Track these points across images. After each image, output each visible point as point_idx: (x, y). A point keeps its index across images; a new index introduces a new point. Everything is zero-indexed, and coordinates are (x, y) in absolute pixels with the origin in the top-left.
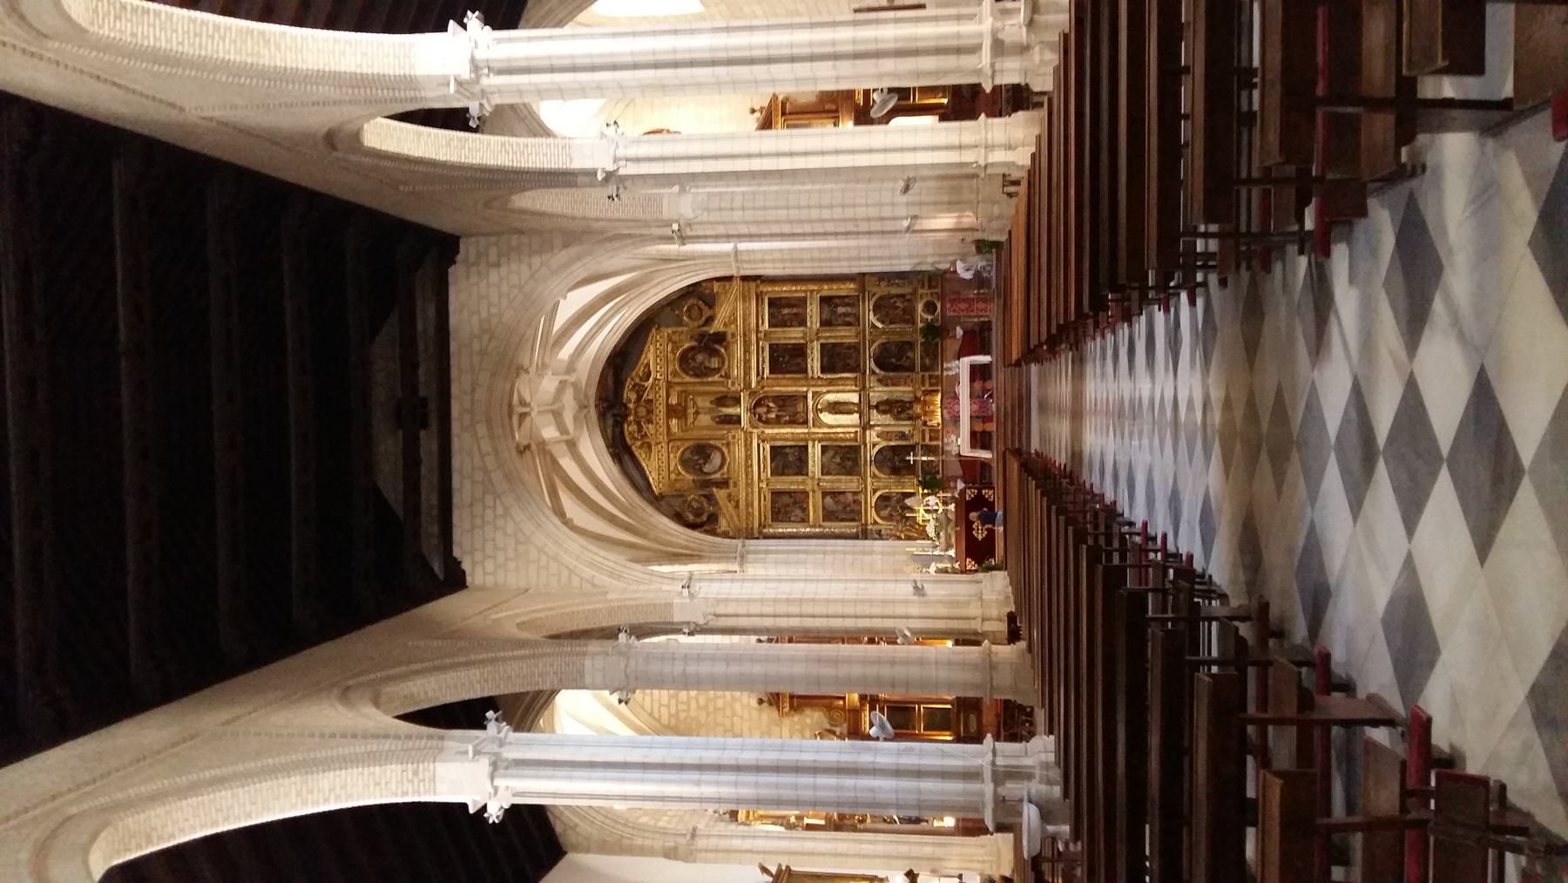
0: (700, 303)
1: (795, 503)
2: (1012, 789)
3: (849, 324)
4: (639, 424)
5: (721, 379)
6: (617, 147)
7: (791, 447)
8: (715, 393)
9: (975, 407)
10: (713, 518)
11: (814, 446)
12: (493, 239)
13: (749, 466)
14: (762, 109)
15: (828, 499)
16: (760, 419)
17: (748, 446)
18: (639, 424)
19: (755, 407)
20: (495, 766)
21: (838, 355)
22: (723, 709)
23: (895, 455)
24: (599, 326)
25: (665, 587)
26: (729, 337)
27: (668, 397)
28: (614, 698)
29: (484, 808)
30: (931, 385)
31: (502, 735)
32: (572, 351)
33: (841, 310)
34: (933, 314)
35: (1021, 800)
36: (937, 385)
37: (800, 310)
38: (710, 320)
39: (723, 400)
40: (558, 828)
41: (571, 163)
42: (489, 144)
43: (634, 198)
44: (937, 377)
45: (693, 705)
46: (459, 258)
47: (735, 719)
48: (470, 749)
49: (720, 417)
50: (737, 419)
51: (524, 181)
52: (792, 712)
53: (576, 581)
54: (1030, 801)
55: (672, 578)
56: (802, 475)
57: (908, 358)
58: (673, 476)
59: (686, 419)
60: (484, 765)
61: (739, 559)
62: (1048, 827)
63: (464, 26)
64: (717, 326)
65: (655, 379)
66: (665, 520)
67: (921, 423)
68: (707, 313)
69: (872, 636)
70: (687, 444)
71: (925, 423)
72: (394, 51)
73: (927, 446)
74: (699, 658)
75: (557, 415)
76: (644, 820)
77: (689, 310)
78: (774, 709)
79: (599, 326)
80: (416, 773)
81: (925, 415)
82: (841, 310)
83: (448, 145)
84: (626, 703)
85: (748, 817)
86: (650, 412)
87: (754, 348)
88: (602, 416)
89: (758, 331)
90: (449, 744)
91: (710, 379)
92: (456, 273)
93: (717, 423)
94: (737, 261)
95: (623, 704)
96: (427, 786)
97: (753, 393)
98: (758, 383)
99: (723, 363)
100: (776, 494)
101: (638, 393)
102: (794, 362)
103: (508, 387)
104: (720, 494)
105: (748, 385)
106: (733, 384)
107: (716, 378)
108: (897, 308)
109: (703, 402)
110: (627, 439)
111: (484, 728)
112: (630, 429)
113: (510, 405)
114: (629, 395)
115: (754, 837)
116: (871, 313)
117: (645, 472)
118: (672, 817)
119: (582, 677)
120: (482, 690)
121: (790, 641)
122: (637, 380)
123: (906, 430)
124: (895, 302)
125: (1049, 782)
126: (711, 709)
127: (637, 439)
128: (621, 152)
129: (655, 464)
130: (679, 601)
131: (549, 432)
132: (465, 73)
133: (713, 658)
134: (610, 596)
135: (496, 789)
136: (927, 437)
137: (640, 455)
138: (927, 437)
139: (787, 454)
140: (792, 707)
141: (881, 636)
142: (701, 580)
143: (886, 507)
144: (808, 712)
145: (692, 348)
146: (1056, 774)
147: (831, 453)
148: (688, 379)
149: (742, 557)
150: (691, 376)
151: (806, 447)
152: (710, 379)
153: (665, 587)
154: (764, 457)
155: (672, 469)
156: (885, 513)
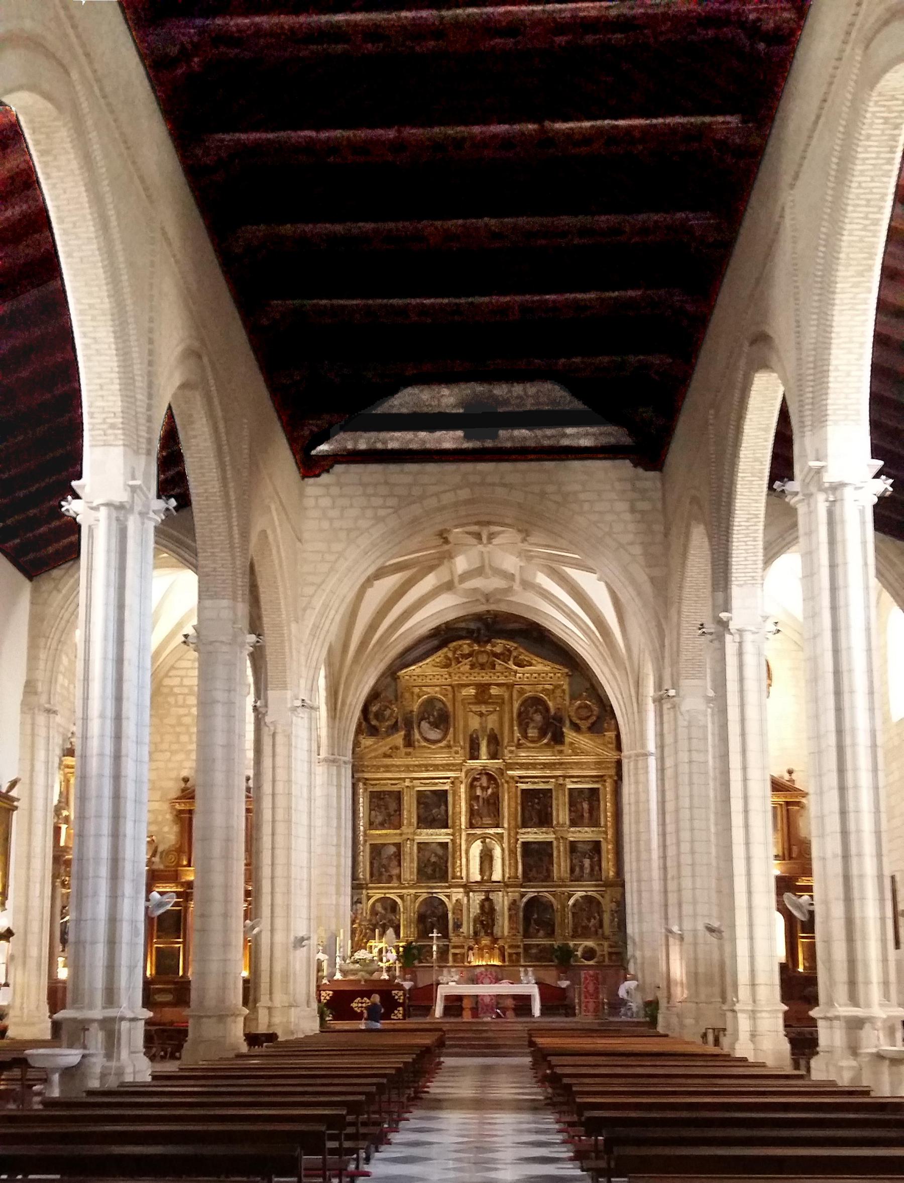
0: (594, 718)
1: (389, 815)
3: (572, 870)
4: (470, 655)
6: (754, 633)
7: (447, 811)
8: (502, 733)
9: (487, 1000)
10: (373, 731)
14: (793, 781)
15: (393, 850)
16: (475, 779)
17: (447, 767)
18: (470, 655)
19: (487, 774)
20: (120, 507)
21: (541, 860)
22: (178, 742)
23: (439, 918)
25: (302, 682)
26: (559, 748)
27: (498, 685)
29: (77, 496)
30: (510, 955)
31: (152, 515)
32: (545, 587)
33: (587, 862)
34: (583, 957)
36: (510, 961)
37: (586, 821)
38: (576, 728)
39: (495, 741)
40: (56, 573)
41: (738, 585)
42: (756, 501)
43: (701, 650)
44: (518, 961)
45: (182, 711)
46: (640, 471)
48: (138, 482)
49: (477, 738)
50: (474, 756)
52: (175, 813)
53: (309, 590)
54: (84, 1056)
55: (313, 689)
56: (418, 823)
57: (538, 931)
58: (417, 690)
60: (122, 496)
61: (332, 757)
63: (877, 476)
64: (570, 735)
67: (471, 944)
68: (584, 725)
69: (253, 894)
70: (449, 705)
71: (470, 948)
73: (448, 950)
75: (479, 571)
76: (65, 660)
77: (587, 706)
78: (179, 794)
81: (479, 949)
82: (587, 862)
83: (756, 460)
84: (184, 642)
85: (68, 767)
86: (482, 666)
87: (548, 773)
88: (478, 617)
89: (565, 777)
90: (143, 460)
91: (516, 728)
92: (625, 467)
94: (637, 755)
95: (183, 639)
96: (99, 438)
98: (512, 777)
99: (532, 742)
101: (502, 654)
102: (534, 814)
103: (508, 521)
104: (398, 739)
105: (510, 766)
106: (511, 752)
107: (517, 735)
108: (589, 920)
109: (492, 722)
110: (454, 644)
112: (465, 646)
113: (489, 523)
114: (499, 645)
116: (584, 893)
118: (68, 689)
119: (211, 597)
120: (198, 495)
122: (515, 654)
123: (464, 929)
124: (595, 918)
126: (178, 729)
131: (461, 564)
132: (828, 478)
133: (230, 731)
134: (294, 626)
135: (96, 509)
136: (457, 951)
137: (439, 656)
138: (457, 951)
139: (439, 807)
142: (310, 719)
145: (547, 709)
147: (440, 852)
148: (516, 705)
151: (446, 827)
152: (516, 728)
154: (437, 784)
155: (424, 689)
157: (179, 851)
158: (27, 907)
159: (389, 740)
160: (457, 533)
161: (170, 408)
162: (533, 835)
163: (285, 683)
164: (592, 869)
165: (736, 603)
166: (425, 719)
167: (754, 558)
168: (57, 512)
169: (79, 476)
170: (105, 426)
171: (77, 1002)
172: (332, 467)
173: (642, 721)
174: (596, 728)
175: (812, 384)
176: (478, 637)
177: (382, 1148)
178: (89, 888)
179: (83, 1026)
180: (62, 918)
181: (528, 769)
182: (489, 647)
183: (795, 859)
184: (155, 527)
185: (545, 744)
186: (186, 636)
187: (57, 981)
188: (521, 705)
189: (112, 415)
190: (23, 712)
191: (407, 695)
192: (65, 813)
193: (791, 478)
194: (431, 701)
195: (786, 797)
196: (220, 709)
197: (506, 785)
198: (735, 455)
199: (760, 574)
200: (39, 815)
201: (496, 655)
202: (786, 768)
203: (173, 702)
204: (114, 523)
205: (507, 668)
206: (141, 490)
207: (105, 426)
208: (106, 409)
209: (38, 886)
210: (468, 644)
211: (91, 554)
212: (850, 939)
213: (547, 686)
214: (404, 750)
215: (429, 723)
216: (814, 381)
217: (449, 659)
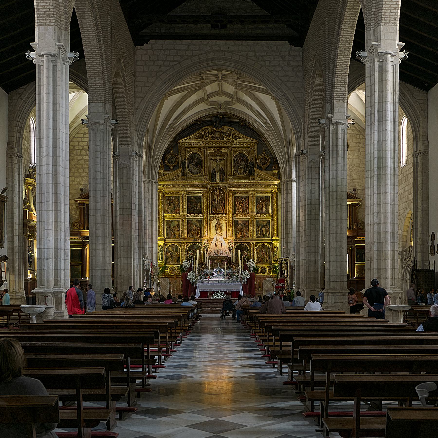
0: (268, 164)
1: (174, 207)
2: (51, 301)
3: (257, 233)
4: (212, 133)
5: (233, 173)
6: (342, 124)
7: (201, 206)
8: (226, 170)
10: (167, 168)
11: (201, 216)
12: (301, 54)
13: (192, 185)
14: (356, 194)
15: (176, 223)
16: (214, 191)
17: (201, 185)
18: (212, 133)
19: (219, 189)
20: (54, 56)
22: (78, 172)
24: (259, 115)
25: (136, 144)
26: (252, 177)
27: (225, 147)
28: (84, 117)
29: (33, 51)
31: (68, 60)
32: (247, 101)
33: (264, 230)
34: (261, 272)
35: (46, 304)
38: (259, 168)
39: (223, 173)
40: (20, 90)
41: (336, 102)
42: (346, 62)
43: (318, 132)
45: (79, 158)
46: (292, 46)
47: (74, 178)
48: (61, 44)
49: (215, 172)
50: (214, 180)
51: (328, 79)
52: (77, 205)
53: (139, 100)
54: (46, 308)
55: (140, 147)
56: (188, 211)
58: (187, 149)
59: (214, 156)
60: (53, 50)
61: (148, 180)
62: (35, 316)
63: (401, 51)
64: (257, 171)
65: (233, 142)
66: (167, 145)
68: (264, 167)
69: (115, 242)
70: (203, 157)
72: (392, 15)
74: (104, 158)
75: (217, 93)
76: (25, 133)
77: (265, 158)
78: (79, 196)
79: (259, 115)
80: (49, 15)
82: (264, 230)
83: (347, 42)
84: (82, 123)
85: (28, 183)
86: (218, 139)
87: (247, 189)
88: (216, 116)
89: (254, 191)
90: (63, 32)
91: (233, 168)
92: (285, 45)
93: (213, 170)
94: (287, 181)
95: (81, 122)
96: (42, 21)
97: (226, 188)
98: (231, 190)
99: (240, 174)
100: (178, 198)
101: (227, 133)
103: (231, 69)
104: (179, 171)
105: (230, 185)
106: (230, 179)
107: (233, 171)
109: (222, 165)
110: (205, 127)
111: (71, 51)
112: (210, 128)
113: (222, 70)
114: (226, 128)
115: (19, 185)
117: (189, 135)
118: (27, 146)
119: (94, 102)
120: (87, 52)
121: (112, 204)
122: (232, 133)
125: (55, 317)
126: (78, 166)
127: (205, 132)
128: (340, 126)
129: (193, 141)
130: (130, 150)
131: (209, 89)
132: (381, 50)
133: (104, 165)
134: (132, 117)
135: (42, 56)
137: (197, 134)
140: (80, 204)
141: (115, 247)
142: (139, 161)
143: (173, 250)
144: (78, 212)
145: (247, 160)
146: (58, 319)
148: (233, 157)
149: (150, 182)
150: (234, 159)
151: (201, 213)
152: (233, 168)
153: (136, 144)
154: (196, 193)
155: (191, 149)
156: (170, 249)
157: (80, 222)
158: (13, 247)
159: (174, 172)
160: (207, 74)
161: (74, 8)
162: (240, 217)
163: (128, 144)
164: (266, 233)
165: (335, 110)
166: (191, 163)
167: (344, 89)
168: (24, 58)
169: (34, 41)
170: (45, 15)
171: (41, 286)
172: (149, 41)
173: (290, 166)
174: (269, 169)
175: (375, 5)
176: (215, 125)
177: (160, 370)
178: (45, 233)
179: (45, 295)
180: (29, 252)
181: (238, 187)
182: (221, 130)
183: (354, 229)
184: (69, 66)
185: (246, 175)
186: (83, 120)
187: (28, 280)
188: (235, 157)
189: (48, 10)
190: (7, 157)
191: (183, 151)
192: (28, 204)
193: (364, 50)
194: (194, 154)
195: (352, 201)
196: (99, 155)
197: (228, 194)
198: (337, 40)
199: (346, 97)
200: (16, 205)
201: (224, 133)
202: (353, 188)
203: (75, 154)
204: (51, 63)
205: (229, 140)
206: (63, 47)
207: (45, 15)
208: (45, 7)
209: (17, 237)
210: (212, 128)
211: (40, 78)
212: (379, 260)
213: (247, 149)
214: (181, 177)
215: (193, 164)
216: (376, 3)
217: (202, 135)
